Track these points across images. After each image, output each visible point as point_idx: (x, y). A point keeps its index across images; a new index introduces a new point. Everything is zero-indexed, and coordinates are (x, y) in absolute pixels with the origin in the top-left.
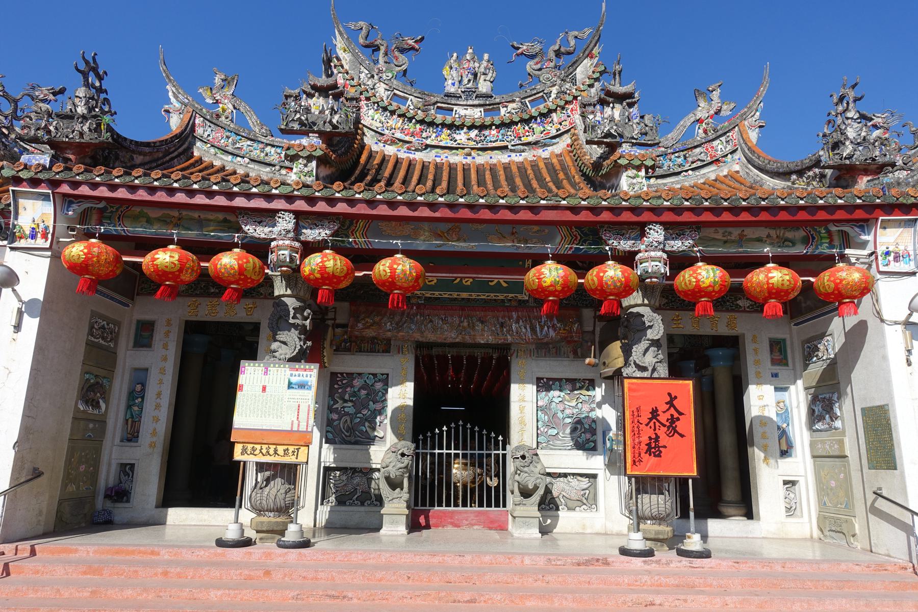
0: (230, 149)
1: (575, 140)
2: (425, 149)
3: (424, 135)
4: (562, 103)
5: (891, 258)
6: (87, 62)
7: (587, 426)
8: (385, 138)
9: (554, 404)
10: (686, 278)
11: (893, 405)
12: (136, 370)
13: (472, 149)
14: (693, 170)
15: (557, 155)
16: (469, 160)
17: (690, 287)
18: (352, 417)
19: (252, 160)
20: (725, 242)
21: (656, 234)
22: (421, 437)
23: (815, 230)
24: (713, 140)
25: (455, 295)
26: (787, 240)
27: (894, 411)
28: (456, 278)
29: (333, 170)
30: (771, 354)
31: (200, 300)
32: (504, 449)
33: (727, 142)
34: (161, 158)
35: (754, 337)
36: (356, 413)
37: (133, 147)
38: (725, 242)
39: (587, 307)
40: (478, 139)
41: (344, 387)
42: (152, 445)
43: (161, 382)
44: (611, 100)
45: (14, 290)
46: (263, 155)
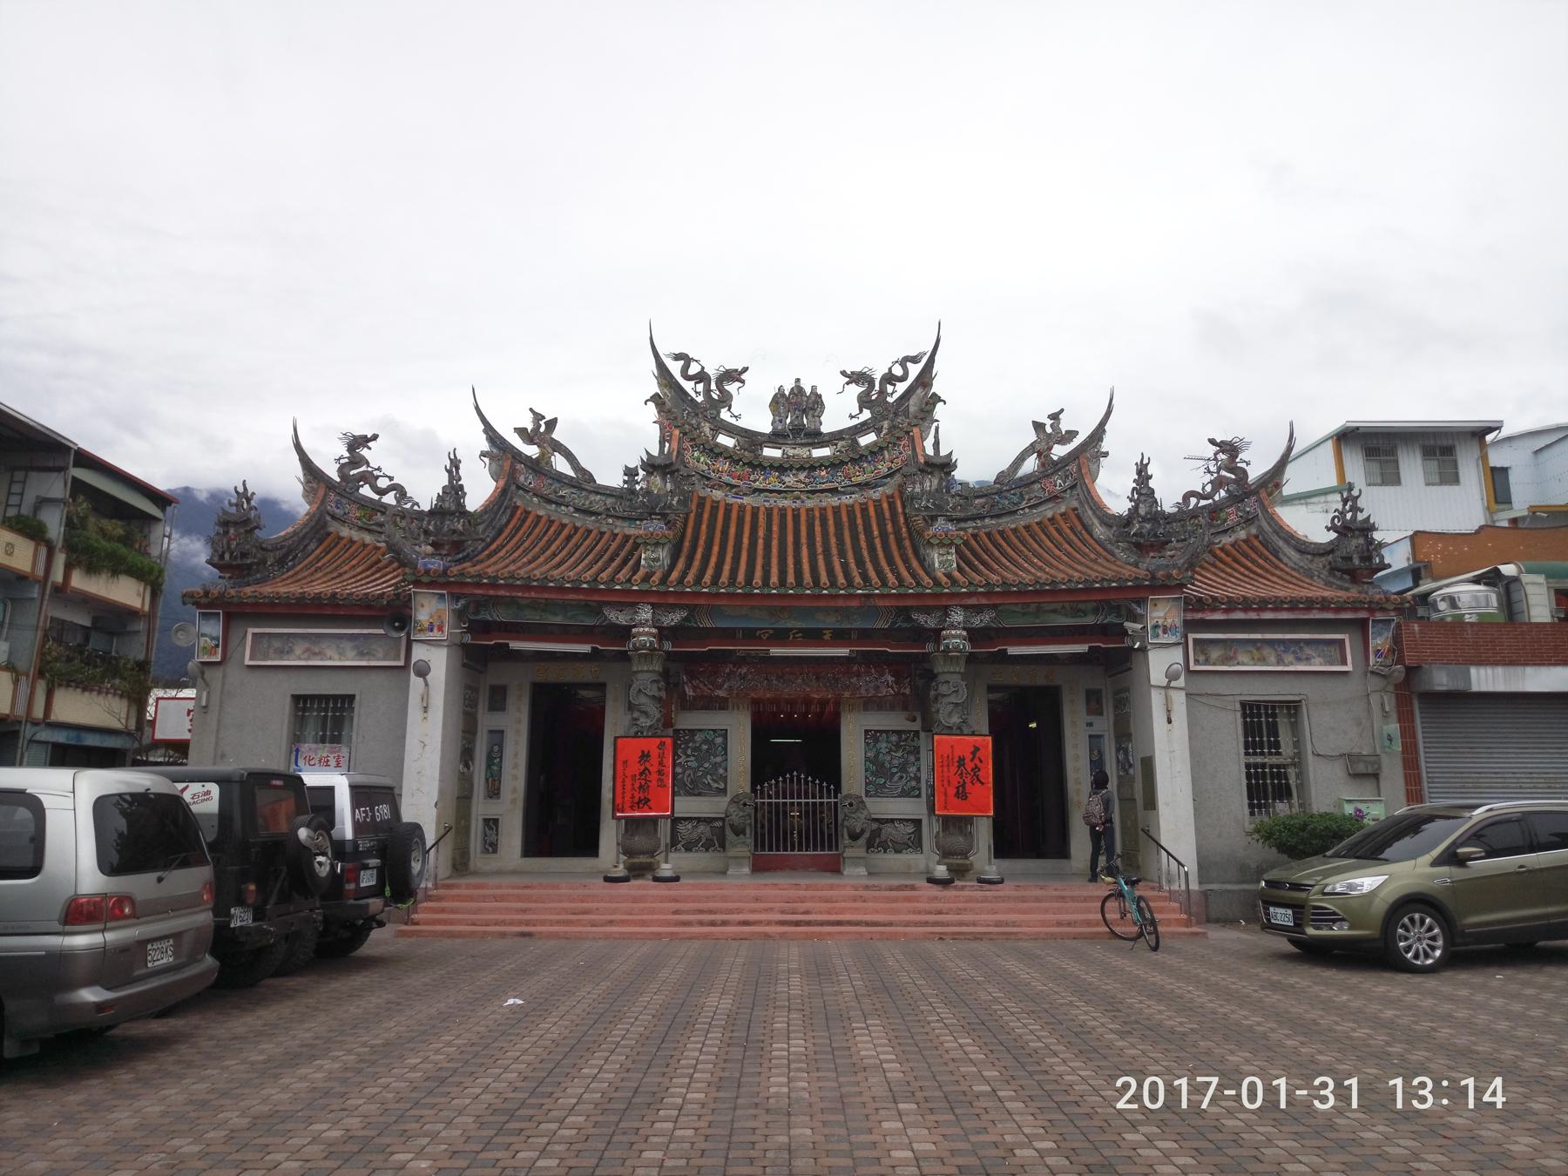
0: (552, 496)
3: (752, 478)
4: (893, 440)
5: (1160, 631)
7: (912, 775)
12: (491, 732)
14: (1029, 507)
18: (695, 770)
19: (577, 510)
21: (957, 617)
22: (759, 787)
26: (1079, 610)
32: (836, 797)
36: (698, 767)
38: (1024, 614)
41: (687, 742)
42: (514, 801)
46: (587, 502)
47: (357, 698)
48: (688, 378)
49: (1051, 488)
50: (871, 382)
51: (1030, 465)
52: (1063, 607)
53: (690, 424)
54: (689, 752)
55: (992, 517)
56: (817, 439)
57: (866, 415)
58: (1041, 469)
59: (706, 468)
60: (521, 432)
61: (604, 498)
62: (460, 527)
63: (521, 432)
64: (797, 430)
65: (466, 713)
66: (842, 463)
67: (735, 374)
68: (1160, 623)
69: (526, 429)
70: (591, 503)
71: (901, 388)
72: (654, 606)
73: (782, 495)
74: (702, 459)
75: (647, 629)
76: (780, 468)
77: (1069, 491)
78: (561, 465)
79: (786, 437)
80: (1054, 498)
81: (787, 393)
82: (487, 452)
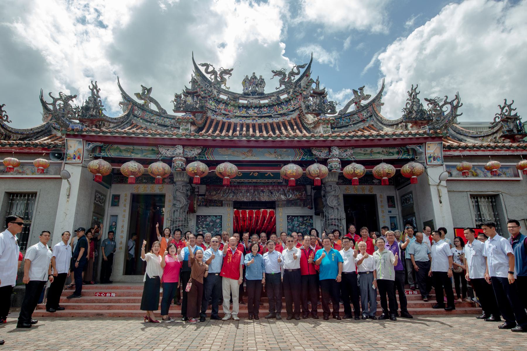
0: (149, 120)
1: (301, 112)
3: (234, 111)
4: (295, 96)
5: (432, 159)
8: (217, 113)
9: (295, 227)
10: (349, 168)
11: (435, 220)
13: (256, 117)
15: (293, 119)
17: (351, 173)
19: (159, 125)
20: (365, 154)
21: (336, 151)
23: (402, 148)
24: (362, 111)
25: (250, 180)
26: (390, 153)
28: (251, 172)
29: (196, 127)
30: (388, 203)
31: (139, 185)
33: (368, 112)
34: (120, 125)
35: (381, 196)
37: (110, 120)
38: (365, 154)
39: (308, 184)
40: (258, 112)
41: (203, 222)
43: (123, 221)
44: (315, 95)
45: (68, 180)
46: (163, 122)
49: (361, 116)
50: (285, 75)
51: (352, 108)
52: (383, 151)
53: (207, 90)
54: (204, 226)
55: (338, 128)
56: (262, 96)
57: (283, 87)
58: (357, 109)
59: (214, 107)
60: (137, 95)
61: (170, 120)
63: (137, 95)
64: (254, 93)
66: (273, 105)
67: (227, 71)
68: (432, 155)
69: (139, 94)
70: (165, 122)
71: (297, 77)
72: (184, 146)
73: (248, 118)
74: (213, 104)
76: (247, 107)
77: (369, 118)
78: (153, 107)
79: (249, 95)
80: (363, 121)
81: (249, 78)
82: (122, 102)
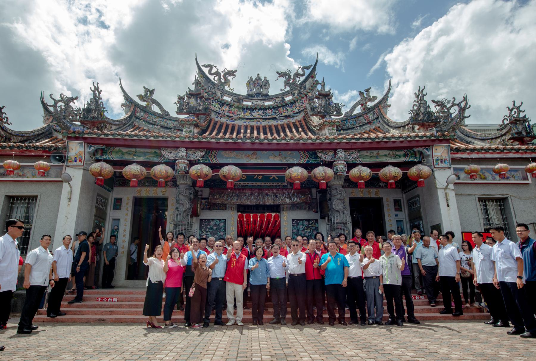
0: (151, 122)
1: (306, 114)
2: (239, 120)
3: (238, 113)
4: (300, 98)
5: (439, 162)
6: (95, 87)
8: (221, 115)
10: (355, 171)
12: (114, 220)
13: (260, 119)
15: (298, 121)
16: (259, 124)
19: (162, 127)
20: (371, 157)
21: (341, 154)
23: (409, 151)
24: (368, 113)
25: (255, 183)
26: (397, 155)
27: (443, 226)
28: (256, 175)
29: (199, 129)
30: (395, 206)
31: (142, 188)
35: (387, 199)
37: (112, 122)
38: (371, 157)
39: (313, 188)
40: (263, 114)
41: (206, 226)
44: (321, 97)
45: (69, 184)
46: (166, 124)
47: (39, 197)
48: (211, 74)
50: (289, 76)
52: (389, 154)
53: (211, 91)
54: (207, 230)
55: (344, 130)
56: (267, 97)
57: (288, 88)
58: (363, 111)
60: (140, 96)
61: (173, 122)
62: (96, 115)
63: (140, 96)
64: (258, 95)
65: (98, 209)
66: (278, 107)
67: (231, 72)
69: (142, 95)
71: (302, 79)
72: (187, 149)
73: (252, 120)
74: (217, 106)
75: (183, 161)
76: (251, 109)
77: (375, 120)
78: (155, 109)
79: (253, 96)
80: (369, 123)
81: (254, 80)
82: (124, 104)
